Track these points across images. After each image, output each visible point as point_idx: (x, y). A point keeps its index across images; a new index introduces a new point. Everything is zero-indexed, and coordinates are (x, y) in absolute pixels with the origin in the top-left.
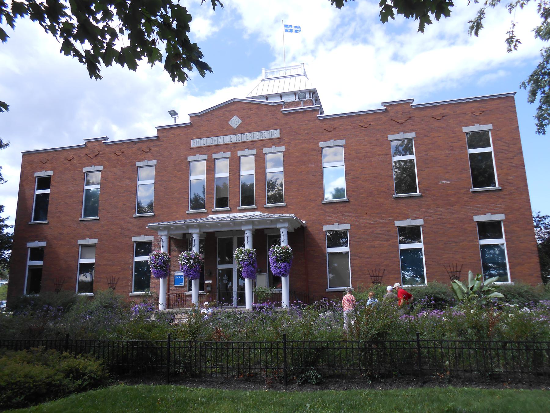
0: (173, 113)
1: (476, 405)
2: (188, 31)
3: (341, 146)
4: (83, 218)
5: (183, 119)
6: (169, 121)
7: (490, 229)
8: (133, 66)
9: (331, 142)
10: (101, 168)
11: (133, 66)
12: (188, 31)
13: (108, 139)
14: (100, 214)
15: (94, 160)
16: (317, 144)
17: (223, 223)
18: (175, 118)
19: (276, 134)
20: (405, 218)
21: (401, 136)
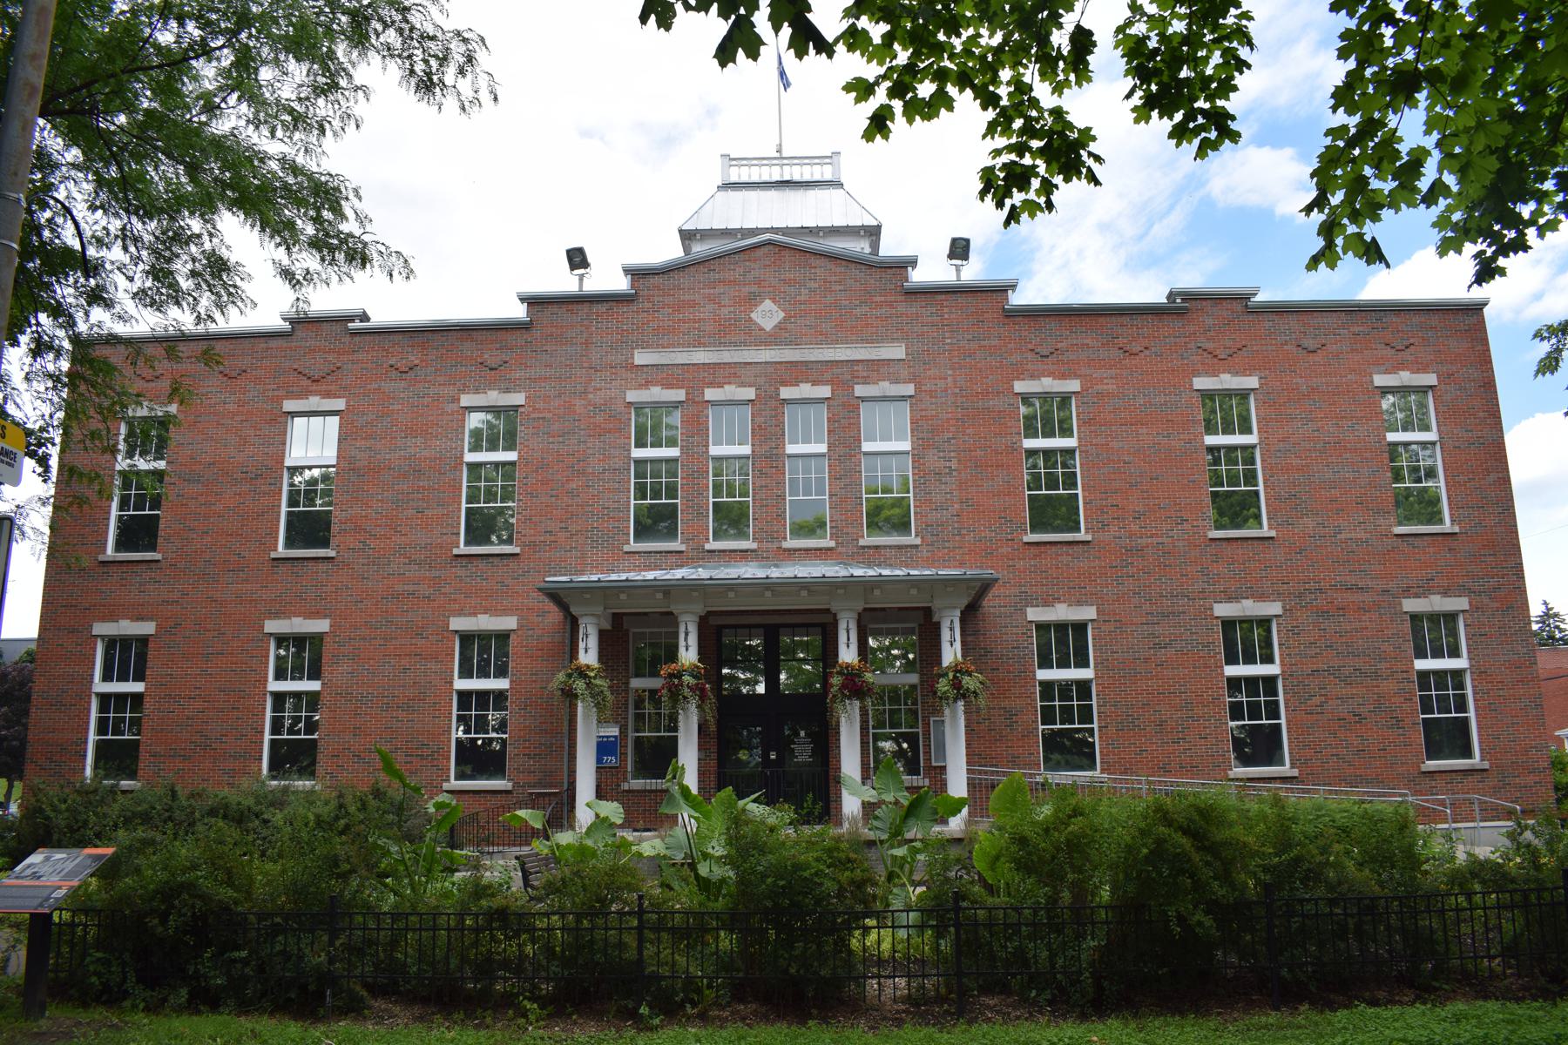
0: (577, 259)
1: (1533, 1032)
2: (810, 11)
3: (903, 398)
4: (463, 549)
5: (606, 278)
6: (564, 282)
7: (1433, 633)
8: (1235, 89)
9: (314, 402)
10: (340, 404)
11: (1235, 89)
12: (810, 11)
13: (364, 317)
14: (333, 542)
15: (1407, 355)
16: (279, 400)
17: (767, 585)
18: (581, 277)
19: (897, 352)
20: (1047, 603)
21: (494, 397)
